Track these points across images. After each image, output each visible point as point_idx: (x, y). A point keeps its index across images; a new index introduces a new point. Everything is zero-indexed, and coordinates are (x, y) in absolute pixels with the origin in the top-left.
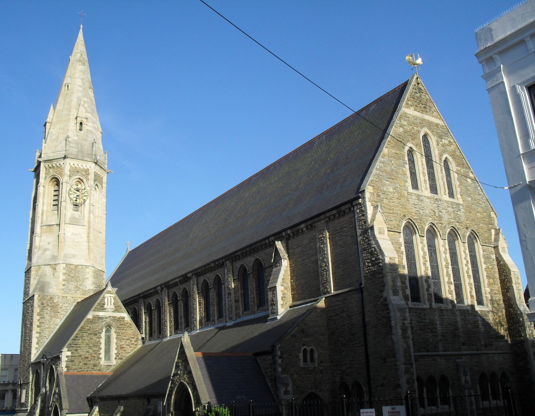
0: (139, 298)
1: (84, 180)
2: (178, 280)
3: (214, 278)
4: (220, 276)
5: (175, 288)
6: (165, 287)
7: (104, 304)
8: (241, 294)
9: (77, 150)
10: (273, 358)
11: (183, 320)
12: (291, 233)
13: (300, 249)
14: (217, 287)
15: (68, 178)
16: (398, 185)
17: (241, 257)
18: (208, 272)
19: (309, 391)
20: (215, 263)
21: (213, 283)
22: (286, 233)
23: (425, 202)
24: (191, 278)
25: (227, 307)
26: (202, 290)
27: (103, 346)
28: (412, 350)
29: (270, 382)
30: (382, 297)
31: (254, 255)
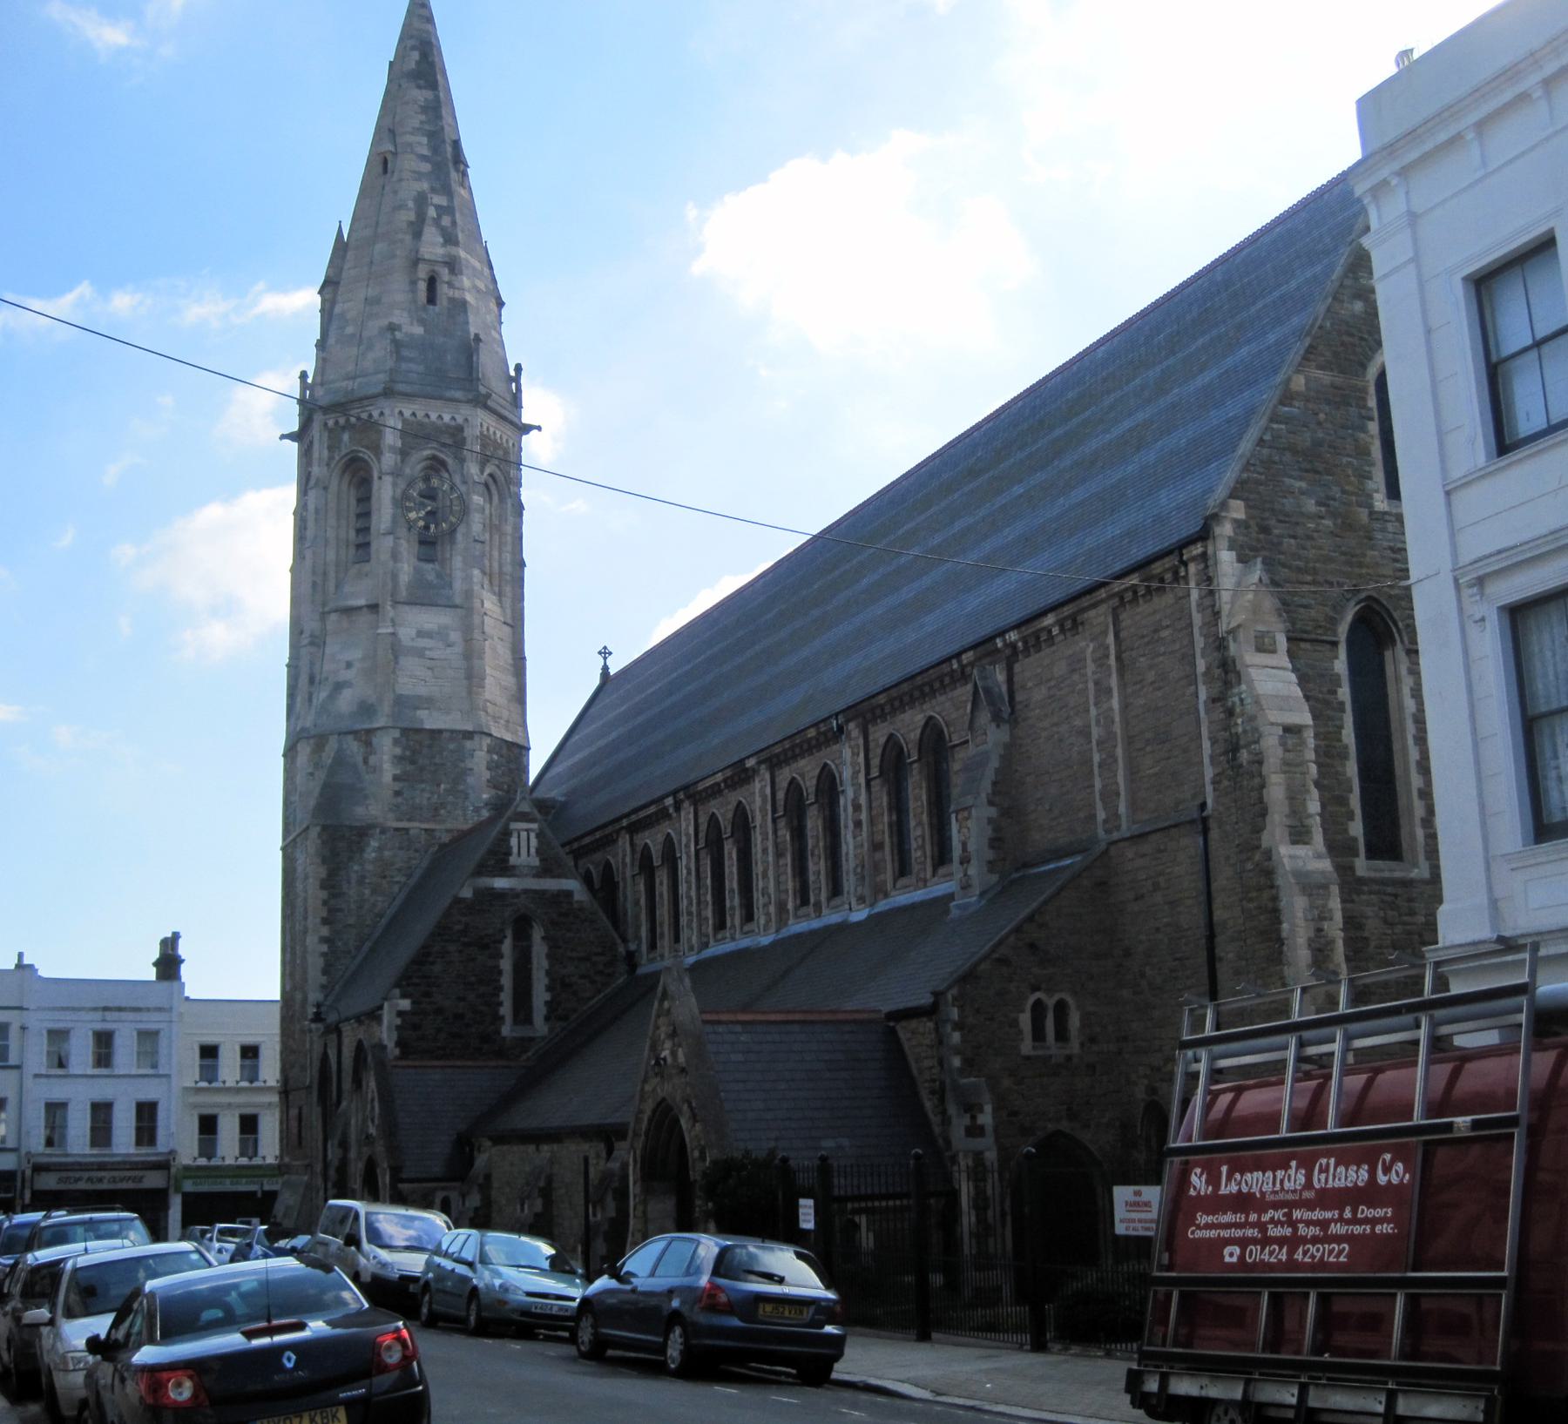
0: (618, 832)
1: (450, 461)
2: (719, 777)
3: (817, 772)
4: (833, 767)
5: (713, 802)
6: (688, 797)
7: (509, 853)
8: (890, 825)
9: (421, 368)
10: (937, 1029)
11: (737, 901)
12: (1020, 639)
14: (826, 801)
15: (399, 457)
16: (1336, 491)
17: (886, 711)
18: (802, 755)
19: (1051, 1127)
20: (818, 728)
22: (1005, 641)
24: (755, 771)
25: (852, 864)
26: (785, 810)
27: (506, 981)
29: (930, 1099)
30: (1258, 847)
31: (925, 707)
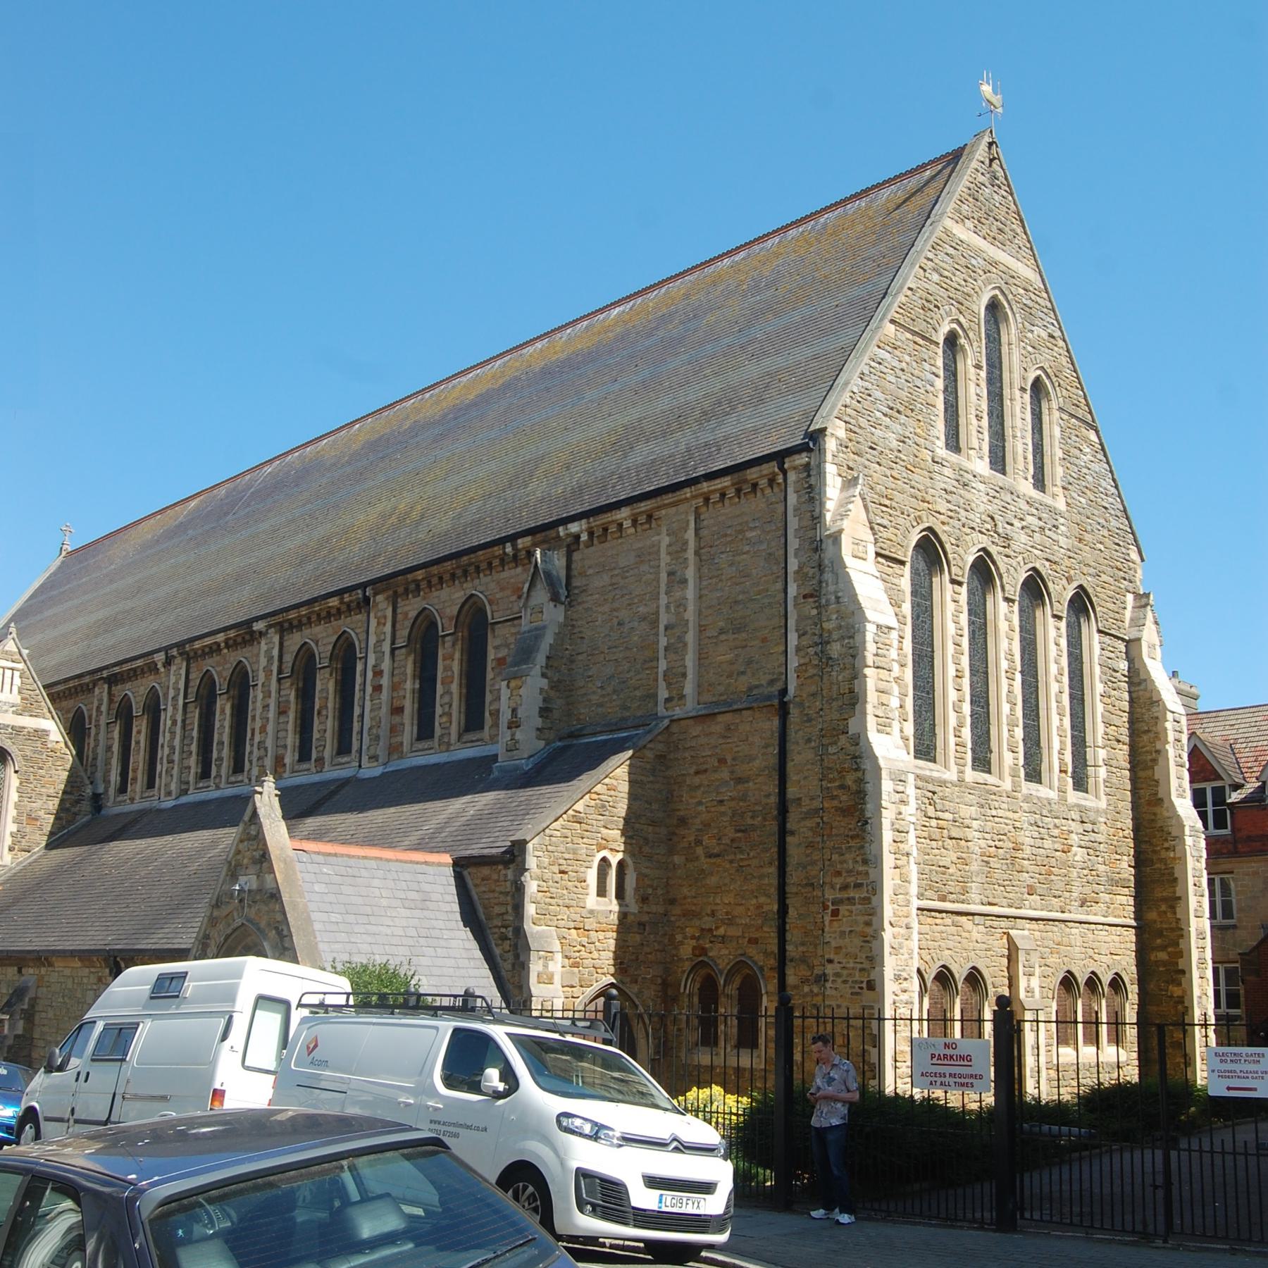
8: (413, 691)
11: (226, 752)
13: (606, 579)
21: (328, 654)
23: (973, 491)
28: (914, 889)
31: (465, 585)
